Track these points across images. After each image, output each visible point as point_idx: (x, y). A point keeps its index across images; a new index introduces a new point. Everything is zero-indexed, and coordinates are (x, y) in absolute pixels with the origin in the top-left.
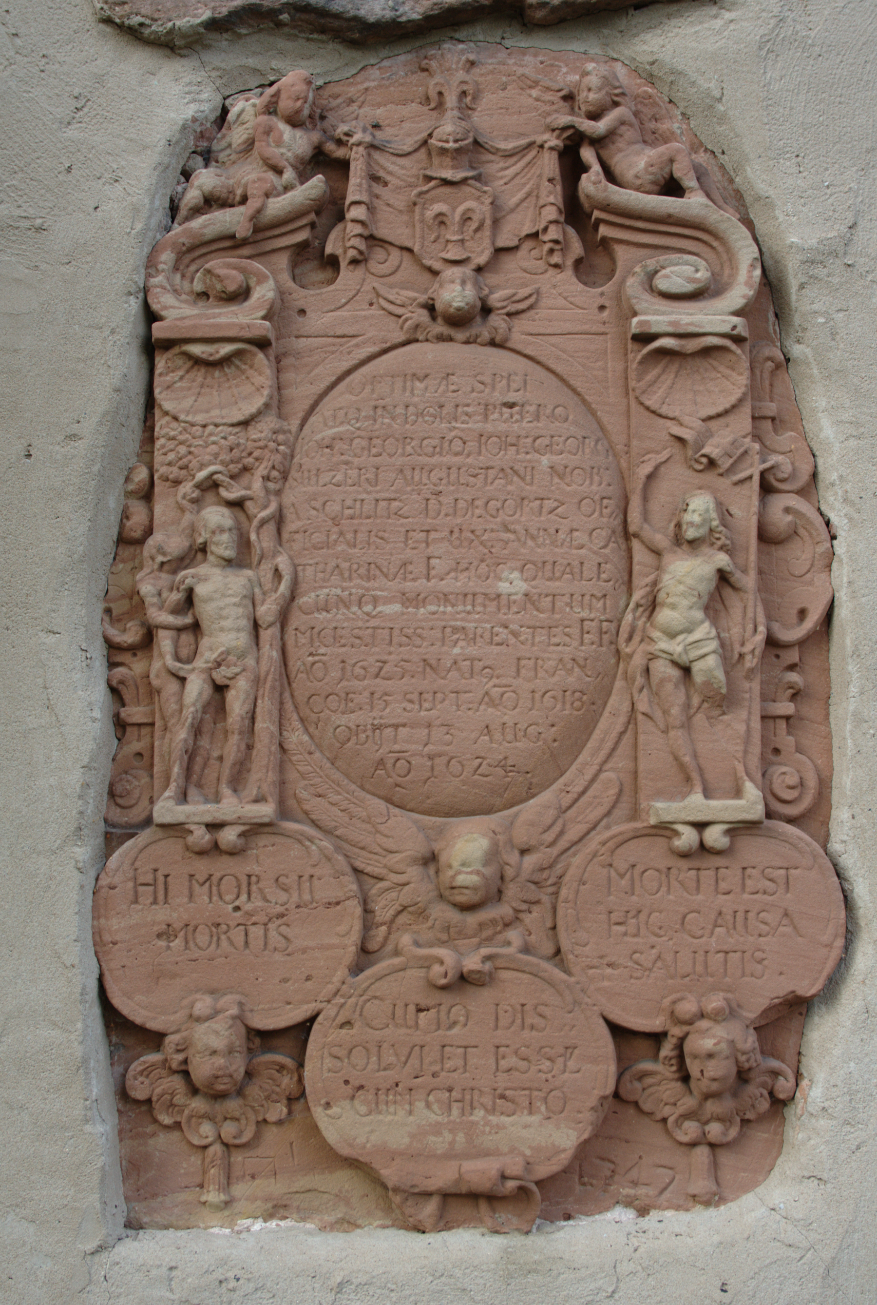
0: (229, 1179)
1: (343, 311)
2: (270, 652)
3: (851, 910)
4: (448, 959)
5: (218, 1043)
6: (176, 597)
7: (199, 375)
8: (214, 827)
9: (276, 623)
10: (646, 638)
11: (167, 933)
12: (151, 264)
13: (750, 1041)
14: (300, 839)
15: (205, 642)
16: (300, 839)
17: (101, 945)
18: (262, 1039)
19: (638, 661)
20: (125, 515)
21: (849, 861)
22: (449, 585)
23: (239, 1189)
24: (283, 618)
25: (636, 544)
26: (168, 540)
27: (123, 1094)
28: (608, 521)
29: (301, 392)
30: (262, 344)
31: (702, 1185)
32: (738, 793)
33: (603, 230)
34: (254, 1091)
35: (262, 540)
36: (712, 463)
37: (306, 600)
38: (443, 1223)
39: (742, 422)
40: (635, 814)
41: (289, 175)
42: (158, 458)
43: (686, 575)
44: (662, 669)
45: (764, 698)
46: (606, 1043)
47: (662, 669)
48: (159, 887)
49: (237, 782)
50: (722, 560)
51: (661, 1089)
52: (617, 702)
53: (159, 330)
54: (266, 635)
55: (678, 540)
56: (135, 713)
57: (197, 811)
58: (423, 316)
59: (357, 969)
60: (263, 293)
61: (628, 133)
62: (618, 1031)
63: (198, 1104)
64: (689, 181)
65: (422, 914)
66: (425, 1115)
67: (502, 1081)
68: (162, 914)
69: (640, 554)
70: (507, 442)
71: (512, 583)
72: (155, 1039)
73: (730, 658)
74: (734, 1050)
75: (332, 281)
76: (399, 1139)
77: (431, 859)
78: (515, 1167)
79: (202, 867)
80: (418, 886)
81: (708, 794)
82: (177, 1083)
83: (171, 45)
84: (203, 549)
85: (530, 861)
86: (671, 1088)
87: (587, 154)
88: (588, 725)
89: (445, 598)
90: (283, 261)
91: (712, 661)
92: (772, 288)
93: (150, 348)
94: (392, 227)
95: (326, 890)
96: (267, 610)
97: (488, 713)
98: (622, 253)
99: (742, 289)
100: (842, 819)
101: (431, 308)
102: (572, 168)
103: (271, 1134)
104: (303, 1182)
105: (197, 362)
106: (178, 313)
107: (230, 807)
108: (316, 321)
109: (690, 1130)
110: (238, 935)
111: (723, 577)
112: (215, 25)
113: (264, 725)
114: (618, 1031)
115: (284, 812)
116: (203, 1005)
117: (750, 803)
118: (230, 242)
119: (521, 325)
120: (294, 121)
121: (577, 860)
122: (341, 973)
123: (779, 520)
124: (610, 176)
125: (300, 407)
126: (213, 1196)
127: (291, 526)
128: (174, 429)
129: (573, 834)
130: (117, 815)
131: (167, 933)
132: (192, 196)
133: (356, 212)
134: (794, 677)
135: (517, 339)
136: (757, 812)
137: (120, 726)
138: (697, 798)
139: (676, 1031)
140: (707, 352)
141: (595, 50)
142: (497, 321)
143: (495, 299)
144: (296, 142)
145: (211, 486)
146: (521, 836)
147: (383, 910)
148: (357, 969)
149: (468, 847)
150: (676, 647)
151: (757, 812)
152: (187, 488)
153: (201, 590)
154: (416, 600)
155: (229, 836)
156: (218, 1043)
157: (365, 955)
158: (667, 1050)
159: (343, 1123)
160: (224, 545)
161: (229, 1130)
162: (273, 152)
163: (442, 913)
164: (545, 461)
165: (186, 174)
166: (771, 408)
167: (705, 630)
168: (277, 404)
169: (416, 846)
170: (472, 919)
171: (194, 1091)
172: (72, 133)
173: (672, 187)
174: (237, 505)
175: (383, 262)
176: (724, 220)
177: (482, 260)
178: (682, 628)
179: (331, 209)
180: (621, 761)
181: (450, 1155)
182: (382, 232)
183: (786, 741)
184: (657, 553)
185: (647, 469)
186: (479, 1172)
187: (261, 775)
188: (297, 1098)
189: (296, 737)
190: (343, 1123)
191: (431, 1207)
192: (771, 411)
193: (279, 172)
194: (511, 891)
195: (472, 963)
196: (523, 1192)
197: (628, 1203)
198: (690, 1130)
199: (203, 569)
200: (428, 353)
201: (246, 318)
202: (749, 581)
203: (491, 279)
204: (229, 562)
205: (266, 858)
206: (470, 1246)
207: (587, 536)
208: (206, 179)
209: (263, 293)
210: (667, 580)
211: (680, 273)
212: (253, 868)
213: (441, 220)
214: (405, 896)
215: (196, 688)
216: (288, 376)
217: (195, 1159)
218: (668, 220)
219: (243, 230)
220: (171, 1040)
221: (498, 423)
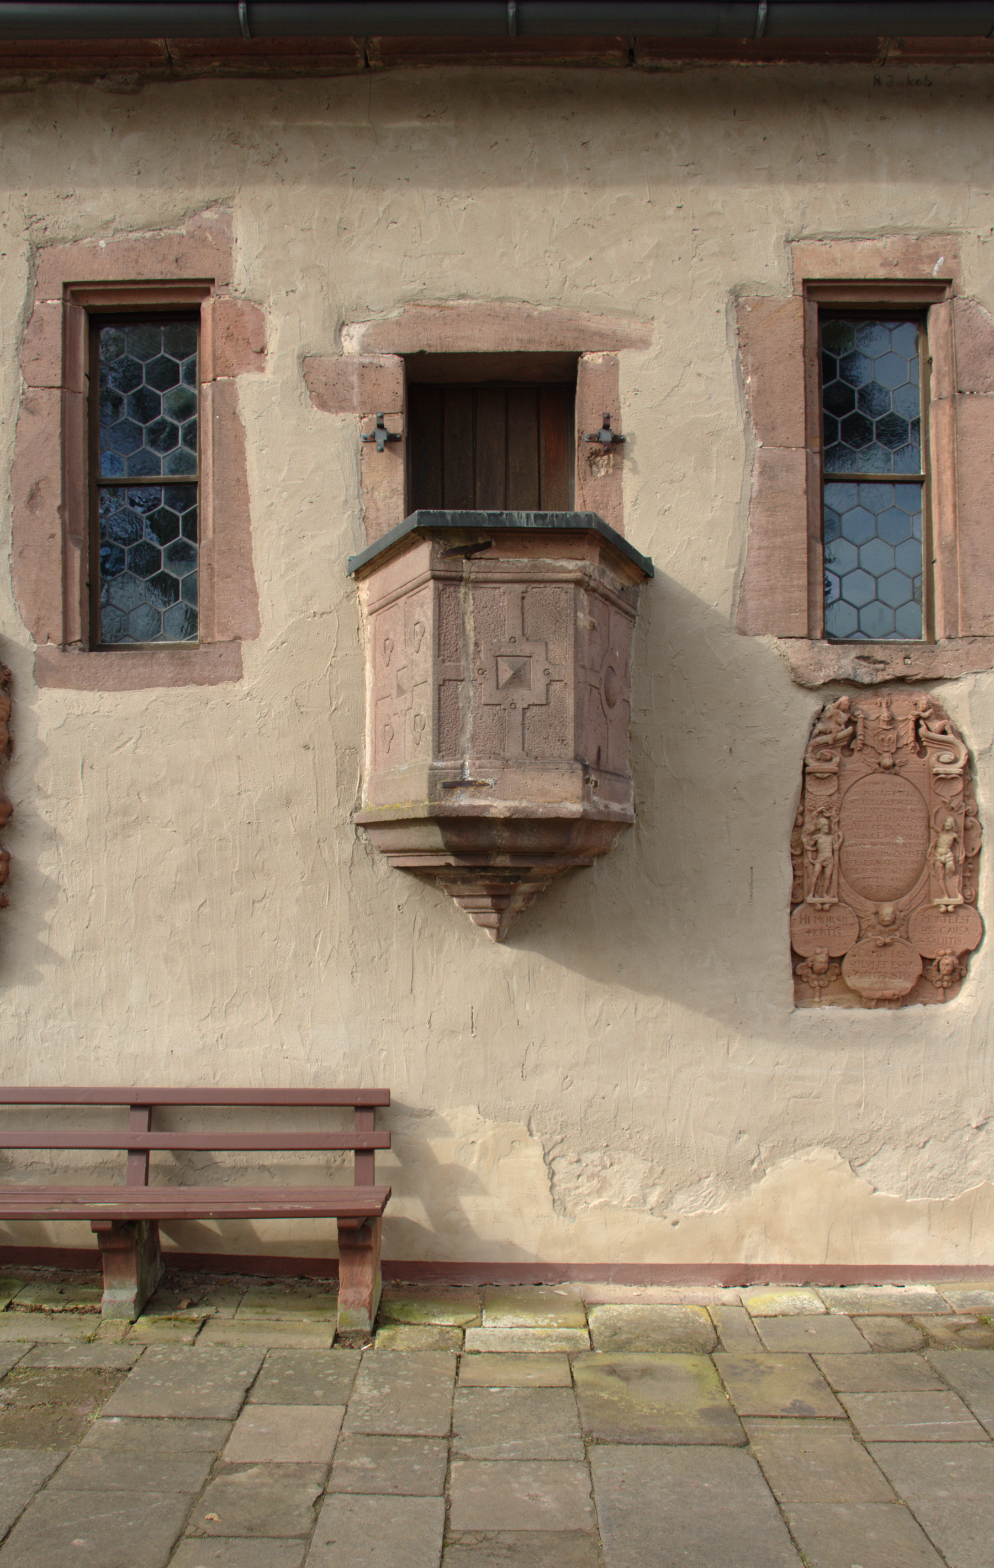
0: (820, 996)
1: (855, 763)
2: (837, 858)
3: (784, 1279)
4: (882, 939)
5: (823, 960)
6: (812, 842)
7: (818, 781)
8: (822, 904)
9: (838, 851)
10: (934, 856)
11: (809, 932)
12: (806, 751)
13: (956, 961)
14: (844, 907)
15: (820, 855)
16: (844, 907)
17: (792, 935)
18: (831, 959)
19: (932, 862)
20: (797, 819)
21: (983, 914)
22: (883, 840)
23: (823, 998)
24: (840, 849)
25: (932, 831)
26: (809, 827)
27: (794, 974)
28: (924, 823)
29: (844, 786)
30: (835, 774)
31: (940, 998)
32: (956, 897)
33: (925, 744)
34: (829, 973)
35: (835, 827)
36: (953, 809)
37: (846, 844)
38: (876, 1007)
39: (961, 797)
40: (929, 901)
41: (843, 726)
42: (806, 804)
43: (946, 839)
44: (939, 864)
45: (964, 872)
46: (920, 962)
47: (939, 864)
48: (807, 920)
49: (827, 892)
50: (955, 835)
51: (934, 975)
52: (925, 872)
53: (808, 769)
54: (836, 853)
55: (943, 829)
56: (799, 873)
57: (817, 900)
58: (877, 766)
59: (857, 942)
60: (836, 760)
61: (933, 716)
62: (923, 958)
63: (814, 976)
64: (949, 731)
65: (874, 927)
66: (873, 979)
67: (893, 971)
68: (807, 927)
69: (933, 833)
70: (899, 802)
71: (900, 840)
72: (803, 959)
73: (956, 861)
74: (953, 964)
75: (851, 755)
76: (867, 985)
77: (876, 913)
78: (897, 992)
79: (818, 914)
80: (873, 920)
81: (949, 897)
82: (809, 970)
83: (812, 689)
84: (819, 830)
85: (902, 914)
86: (935, 973)
87: (921, 722)
88: (917, 878)
89: (882, 844)
90: (839, 749)
91: (951, 863)
92: (969, 764)
93: (804, 774)
94: (870, 742)
95: (850, 921)
96: (836, 846)
97: (892, 875)
98: (929, 750)
99: (962, 762)
100: (981, 904)
101: (879, 764)
102: (917, 726)
103: (832, 984)
104: (839, 996)
105: (818, 778)
106: (813, 765)
107: (827, 899)
108: (849, 767)
109: (939, 984)
110: (827, 932)
111: (955, 840)
112: (824, 684)
113: (835, 877)
114: (923, 958)
115: (840, 901)
116: (818, 950)
117: (959, 899)
118: (826, 745)
119: (903, 769)
120: (844, 711)
121: (914, 914)
122: (853, 942)
123: (969, 824)
124: (928, 729)
125: (844, 790)
126: (817, 999)
127: (842, 823)
128: (811, 797)
129: (913, 907)
130: (795, 901)
131: (809, 932)
132: (816, 731)
133: (861, 737)
134: (971, 866)
135: (902, 773)
136: (962, 902)
137: (795, 876)
138: (946, 898)
139: (938, 958)
140: (953, 778)
141: (923, 691)
142: (897, 768)
143: (897, 761)
144: (844, 717)
145: (821, 812)
146: (901, 907)
147: (864, 926)
148: (857, 942)
149: (887, 910)
150: (943, 858)
151: (962, 902)
152: (815, 813)
153: (820, 841)
154: (875, 844)
155: (827, 906)
156: (823, 960)
157: (859, 938)
158: (935, 963)
159: (852, 981)
160: (826, 829)
161: (821, 983)
162: (839, 720)
163: (879, 927)
164: (909, 807)
165: (814, 725)
166: (967, 793)
167: (950, 854)
168: (838, 790)
169: (873, 910)
170: (887, 929)
171: (813, 972)
172: (785, 714)
173: (944, 732)
174: (828, 818)
175: (867, 751)
176: (957, 742)
177: (893, 751)
178: (944, 854)
179: (853, 736)
180: (926, 888)
181: (880, 989)
182: (867, 742)
183: (968, 883)
184: (937, 833)
185: (935, 810)
186: (888, 993)
187: (834, 890)
188: (840, 974)
189: (842, 880)
190: (852, 981)
191: (874, 1003)
192: (968, 793)
193: (840, 725)
194: (898, 922)
195: (888, 940)
196: (898, 999)
197: (921, 1002)
198: (939, 984)
199: (820, 835)
200: (878, 777)
201: (832, 766)
202: (961, 841)
203: (896, 756)
204: (827, 834)
205: (835, 913)
206: (883, 1013)
207: (920, 828)
208: (820, 727)
209: (836, 760)
210: (941, 840)
211: (947, 757)
212: (831, 915)
213: (883, 740)
214: (870, 923)
215: (818, 868)
216: (841, 782)
217: (812, 990)
218: (943, 741)
219: (831, 742)
220: (810, 959)
221: (897, 796)
